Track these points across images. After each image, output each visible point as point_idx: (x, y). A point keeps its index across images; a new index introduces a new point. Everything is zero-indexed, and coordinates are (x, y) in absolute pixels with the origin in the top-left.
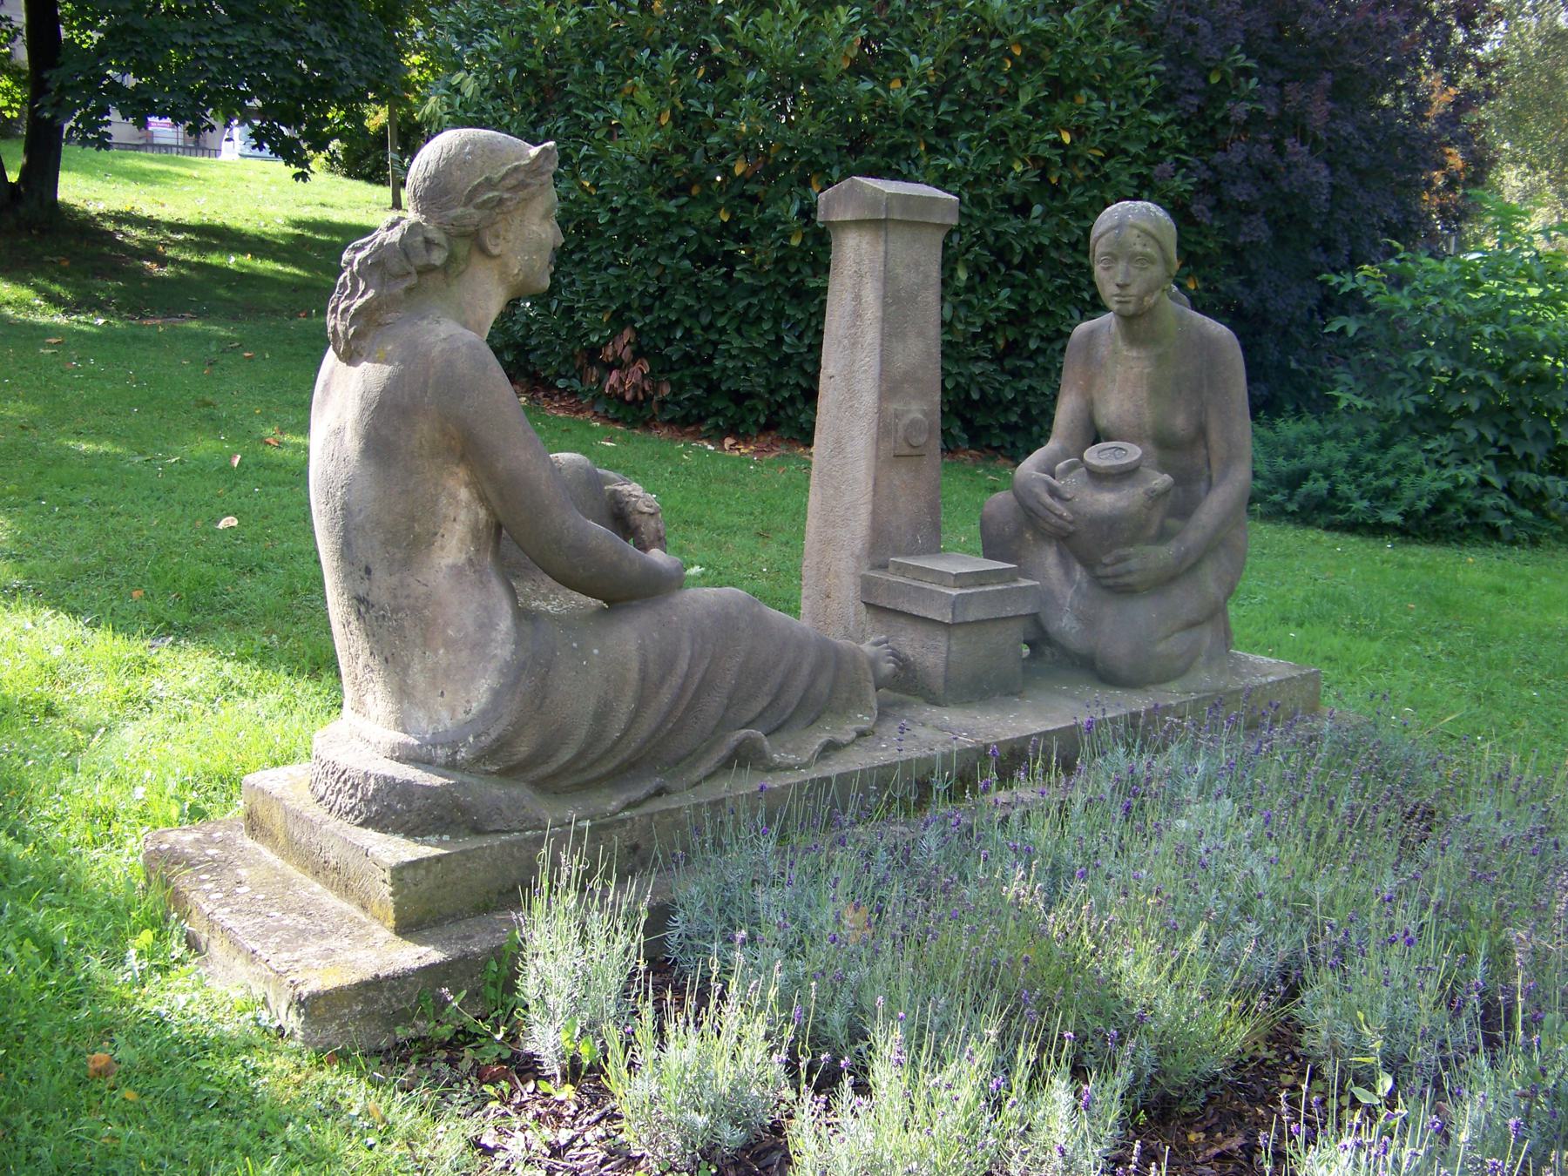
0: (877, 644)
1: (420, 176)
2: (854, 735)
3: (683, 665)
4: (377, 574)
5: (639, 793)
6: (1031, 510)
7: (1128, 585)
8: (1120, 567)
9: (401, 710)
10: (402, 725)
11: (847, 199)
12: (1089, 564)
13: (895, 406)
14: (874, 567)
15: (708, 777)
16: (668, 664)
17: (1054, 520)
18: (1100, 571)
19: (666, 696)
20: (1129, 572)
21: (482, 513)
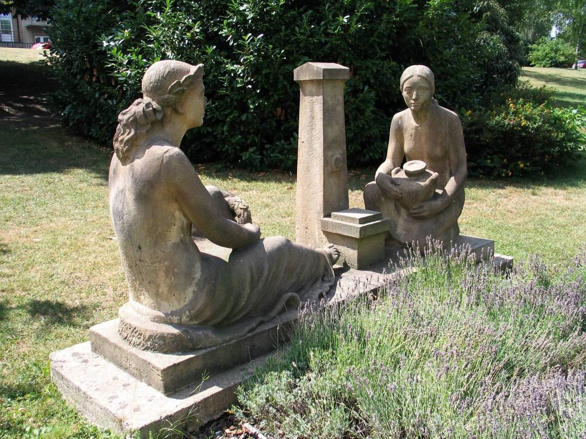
0: (330, 247)
1: (148, 82)
2: (328, 288)
3: (266, 272)
4: (144, 248)
5: (254, 325)
6: (384, 189)
7: (422, 216)
8: (420, 210)
9: (157, 302)
10: (158, 307)
11: (309, 71)
12: (407, 208)
13: (330, 153)
14: (325, 216)
15: (280, 314)
16: (261, 272)
17: (394, 193)
18: (411, 211)
19: (260, 285)
20: (424, 211)
21: (185, 220)
